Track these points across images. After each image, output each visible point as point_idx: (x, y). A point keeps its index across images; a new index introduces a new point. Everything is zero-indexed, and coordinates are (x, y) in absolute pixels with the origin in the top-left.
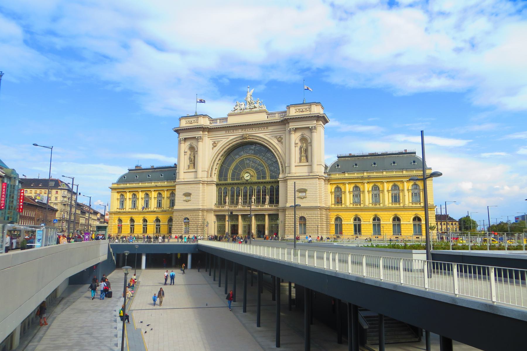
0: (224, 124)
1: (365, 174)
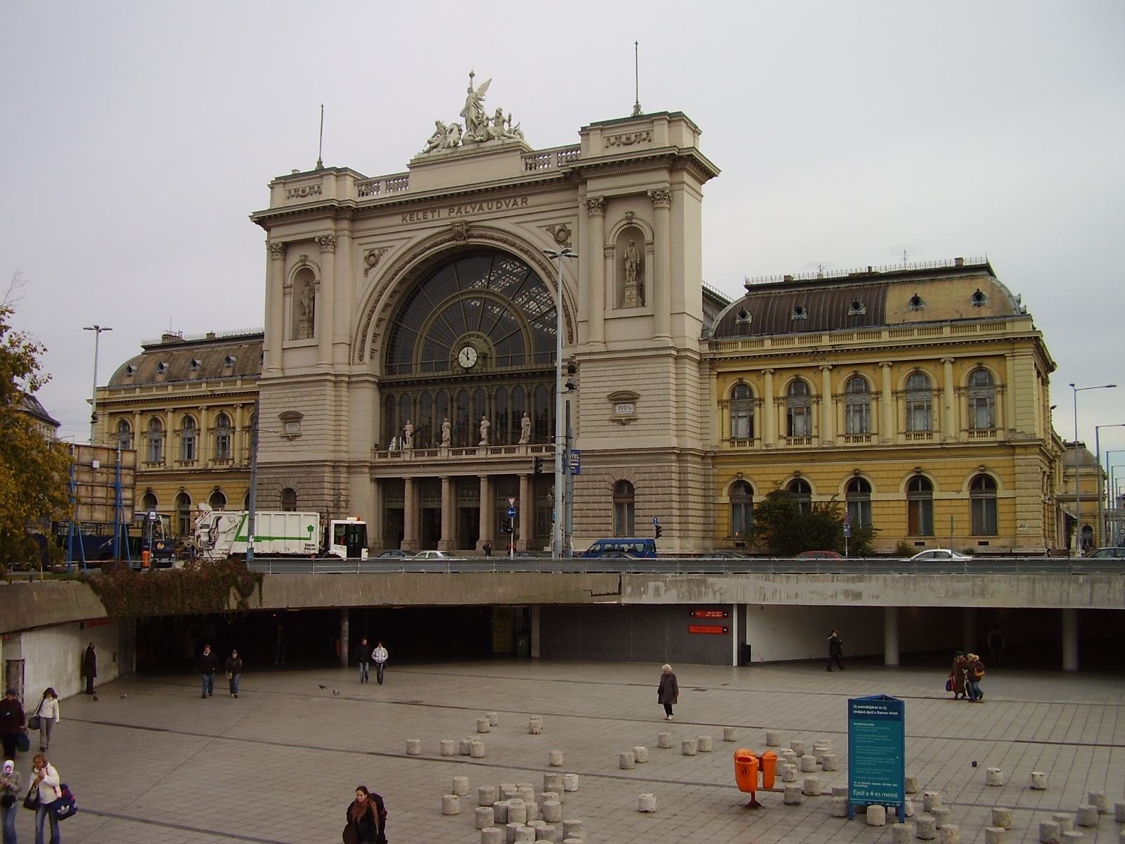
0: (400, 193)
1: (826, 341)
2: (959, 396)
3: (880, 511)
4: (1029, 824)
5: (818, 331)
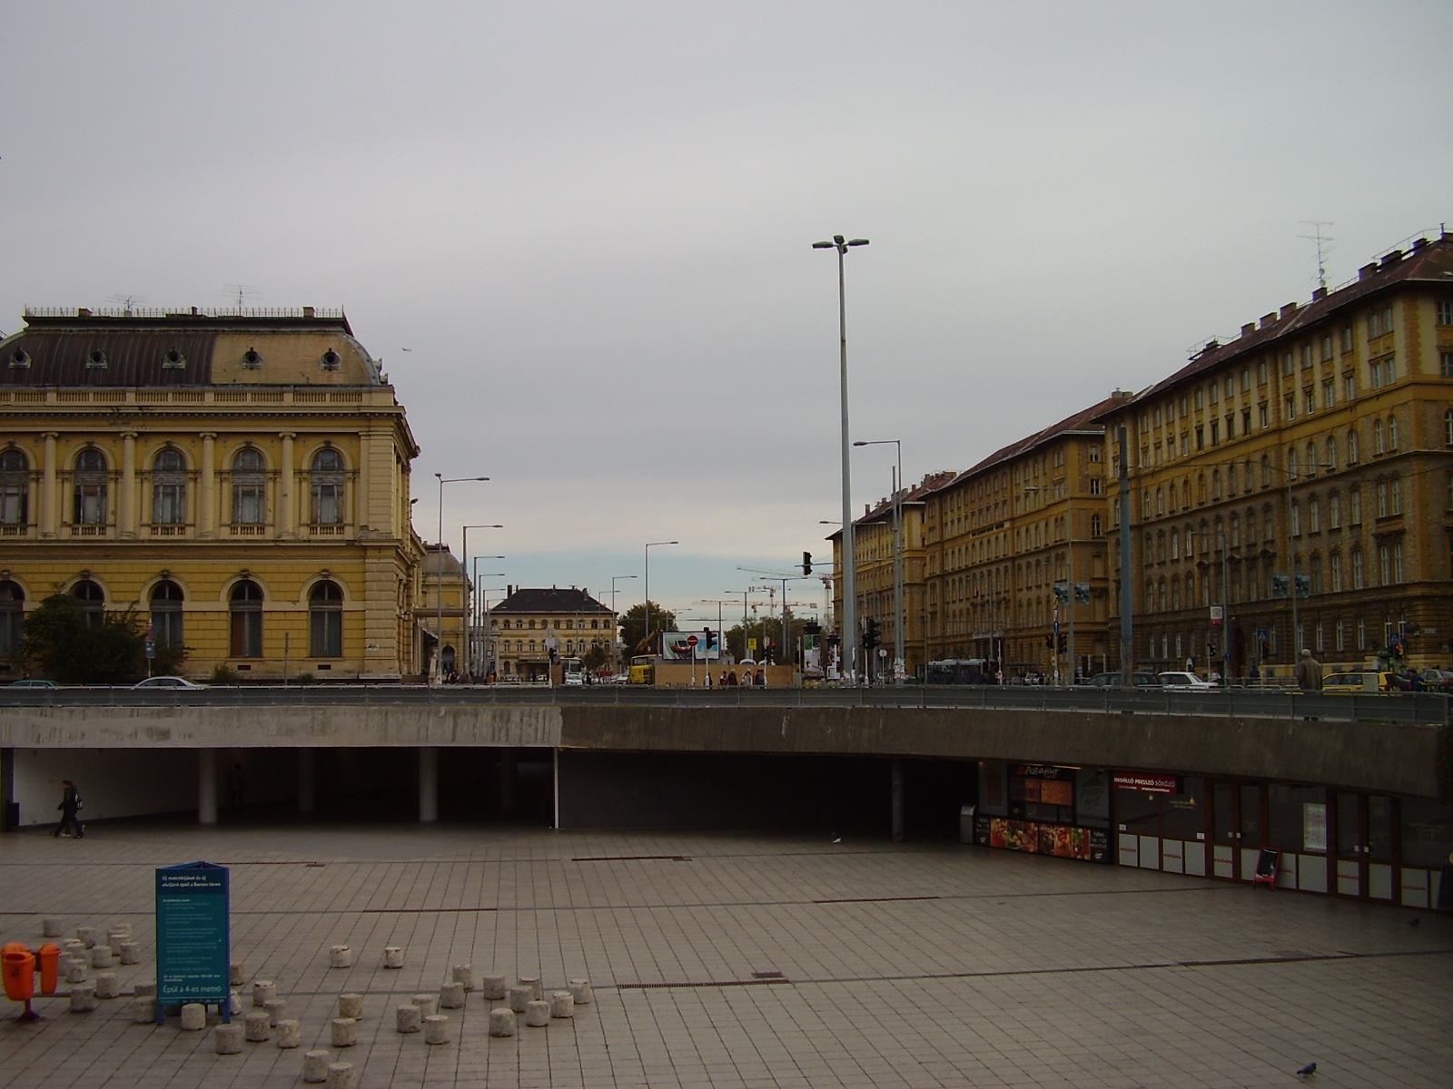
2: (300, 483)
3: (274, 625)
4: (384, 1012)
5: (121, 385)
